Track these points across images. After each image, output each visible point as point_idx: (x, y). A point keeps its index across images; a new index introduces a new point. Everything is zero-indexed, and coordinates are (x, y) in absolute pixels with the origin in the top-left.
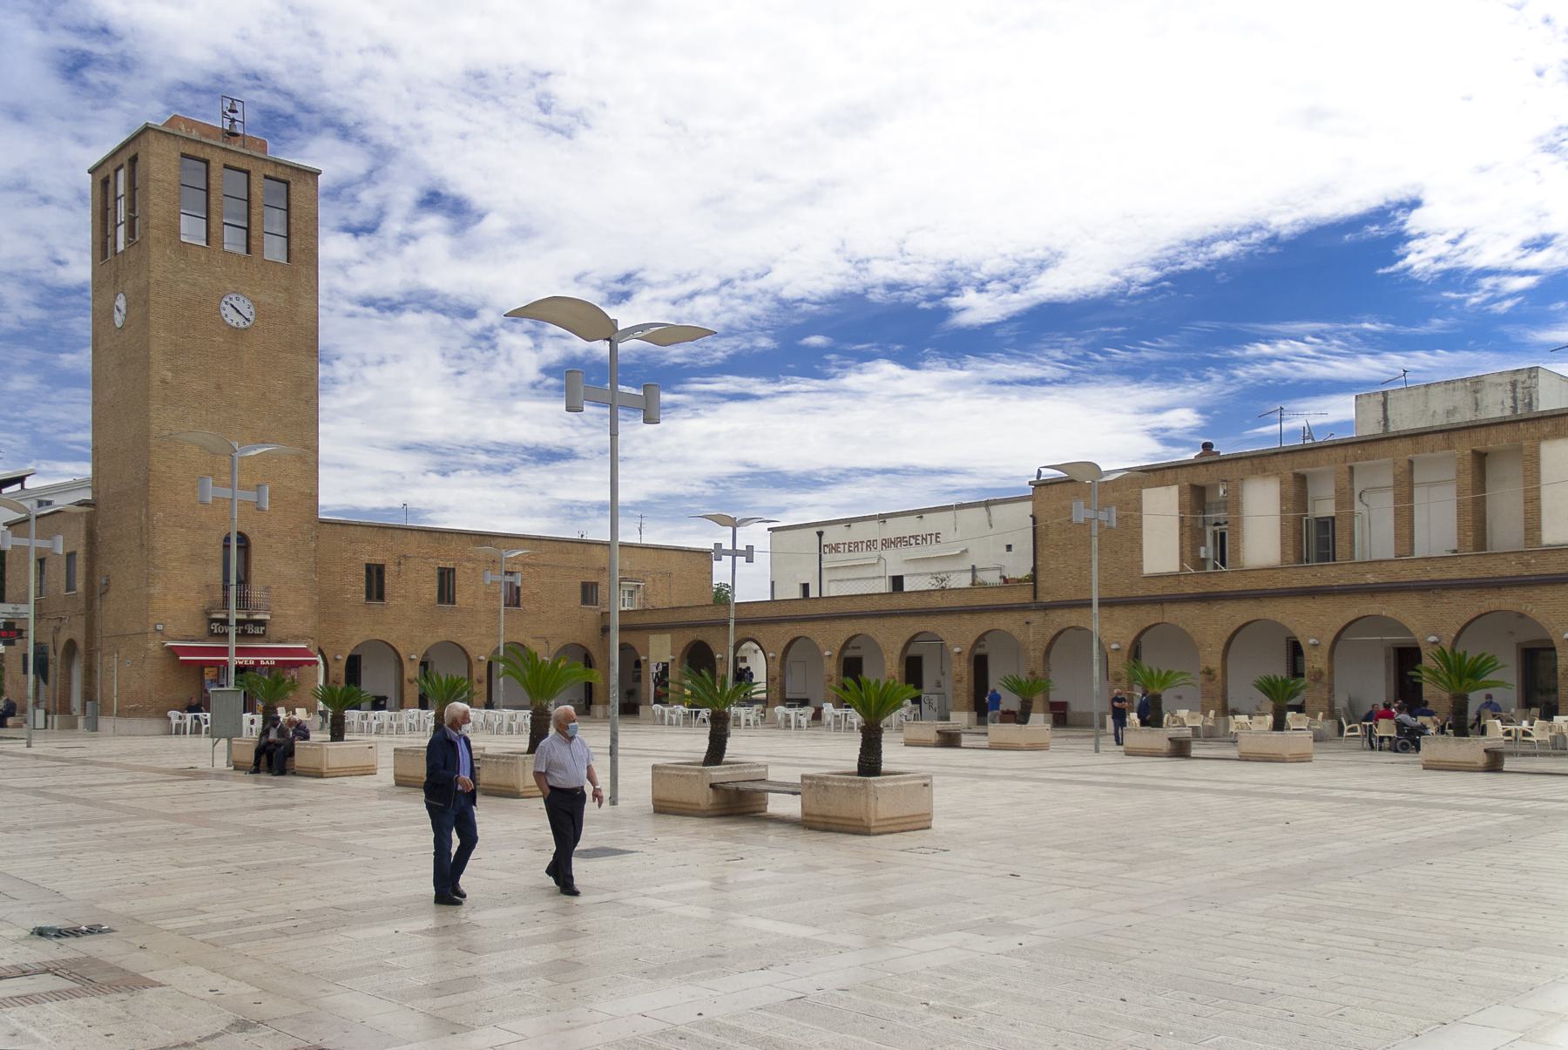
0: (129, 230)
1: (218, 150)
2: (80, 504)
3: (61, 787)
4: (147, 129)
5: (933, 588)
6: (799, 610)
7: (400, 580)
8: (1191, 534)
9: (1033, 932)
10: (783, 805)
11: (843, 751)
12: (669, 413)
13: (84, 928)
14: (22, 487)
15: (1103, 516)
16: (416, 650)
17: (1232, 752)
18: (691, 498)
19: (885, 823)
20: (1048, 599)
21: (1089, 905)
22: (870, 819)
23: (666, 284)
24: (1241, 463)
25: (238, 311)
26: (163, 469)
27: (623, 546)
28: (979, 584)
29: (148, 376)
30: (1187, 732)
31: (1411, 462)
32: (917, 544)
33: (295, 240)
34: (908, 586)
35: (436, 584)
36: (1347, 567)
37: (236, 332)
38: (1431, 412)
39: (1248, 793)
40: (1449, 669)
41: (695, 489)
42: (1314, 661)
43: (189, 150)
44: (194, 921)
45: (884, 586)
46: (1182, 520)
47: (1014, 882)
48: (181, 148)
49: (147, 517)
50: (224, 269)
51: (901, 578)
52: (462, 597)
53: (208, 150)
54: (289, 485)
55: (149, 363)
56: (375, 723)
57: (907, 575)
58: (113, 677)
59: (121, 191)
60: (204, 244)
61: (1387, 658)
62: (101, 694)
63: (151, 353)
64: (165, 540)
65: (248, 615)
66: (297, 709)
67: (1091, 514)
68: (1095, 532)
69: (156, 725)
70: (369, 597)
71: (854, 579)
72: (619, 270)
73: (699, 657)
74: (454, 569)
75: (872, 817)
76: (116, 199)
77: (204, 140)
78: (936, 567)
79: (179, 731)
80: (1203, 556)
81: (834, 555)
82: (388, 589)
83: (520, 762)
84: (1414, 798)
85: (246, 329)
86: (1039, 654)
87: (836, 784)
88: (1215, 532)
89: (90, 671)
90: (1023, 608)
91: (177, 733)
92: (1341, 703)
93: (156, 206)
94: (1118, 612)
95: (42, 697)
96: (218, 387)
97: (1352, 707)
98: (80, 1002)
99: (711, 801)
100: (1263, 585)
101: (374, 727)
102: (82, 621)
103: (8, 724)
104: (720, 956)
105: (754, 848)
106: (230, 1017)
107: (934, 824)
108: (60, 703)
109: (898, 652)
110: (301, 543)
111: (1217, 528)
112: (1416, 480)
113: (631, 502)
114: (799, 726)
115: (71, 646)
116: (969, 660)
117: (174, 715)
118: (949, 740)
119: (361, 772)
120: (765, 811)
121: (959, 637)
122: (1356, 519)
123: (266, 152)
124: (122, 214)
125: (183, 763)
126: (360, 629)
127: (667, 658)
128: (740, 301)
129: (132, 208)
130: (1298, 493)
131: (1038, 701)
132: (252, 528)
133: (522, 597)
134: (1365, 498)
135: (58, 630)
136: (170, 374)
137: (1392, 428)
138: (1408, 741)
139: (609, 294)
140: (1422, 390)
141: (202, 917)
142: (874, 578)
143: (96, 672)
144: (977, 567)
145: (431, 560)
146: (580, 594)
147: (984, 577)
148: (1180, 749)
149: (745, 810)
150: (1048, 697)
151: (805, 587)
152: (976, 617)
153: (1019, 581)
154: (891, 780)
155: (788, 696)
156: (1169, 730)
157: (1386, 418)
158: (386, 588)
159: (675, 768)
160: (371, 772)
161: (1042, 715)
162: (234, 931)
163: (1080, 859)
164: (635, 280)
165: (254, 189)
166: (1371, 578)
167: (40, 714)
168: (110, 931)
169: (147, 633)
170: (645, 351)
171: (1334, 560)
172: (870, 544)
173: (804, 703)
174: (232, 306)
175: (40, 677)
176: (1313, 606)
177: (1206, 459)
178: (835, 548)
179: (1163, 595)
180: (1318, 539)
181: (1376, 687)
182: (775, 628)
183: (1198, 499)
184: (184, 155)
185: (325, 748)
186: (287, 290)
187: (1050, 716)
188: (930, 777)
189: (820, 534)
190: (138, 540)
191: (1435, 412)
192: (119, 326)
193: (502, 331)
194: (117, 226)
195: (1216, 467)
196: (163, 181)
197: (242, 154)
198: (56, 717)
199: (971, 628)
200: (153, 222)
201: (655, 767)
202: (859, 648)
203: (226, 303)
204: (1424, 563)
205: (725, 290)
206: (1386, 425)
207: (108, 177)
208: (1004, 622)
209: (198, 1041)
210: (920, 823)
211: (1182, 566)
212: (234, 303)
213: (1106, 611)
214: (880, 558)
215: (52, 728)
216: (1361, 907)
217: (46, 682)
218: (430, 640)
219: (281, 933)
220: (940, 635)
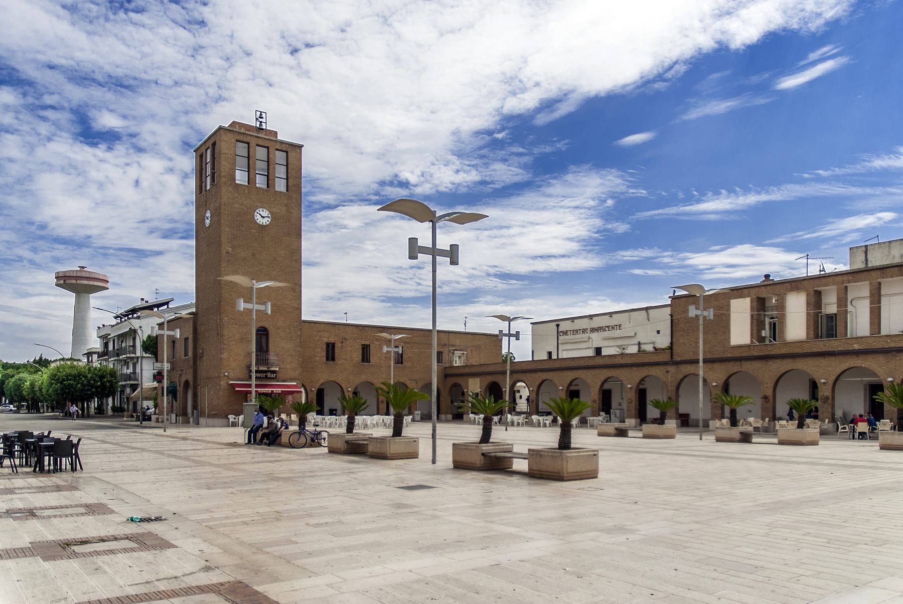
2: (190, 314)
3: (171, 450)
5: (618, 353)
6: (547, 366)
8: (757, 324)
9: (637, 533)
10: (521, 465)
11: (547, 437)
13: (153, 518)
14: (168, 307)
15: (705, 313)
17: (776, 440)
19: (573, 474)
20: (678, 359)
21: (672, 519)
22: (563, 472)
24: (785, 285)
26: (227, 296)
27: (438, 331)
28: (643, 351)
29: (220, 250)
30: (750, 429)
31: (880, 284)
32: (609, 330)
33: (290, 180)
34: (605, 352)
35: (361, 352)
36: (843, 341)
37: (262, 227)
38: (892, 257)
39: (777, 461)
40: (896, 395)
42: (824, 391)
43: (240, 138)
44: (206, 516)
45: (591, 353)
46: (752, 316)
47: (635, 507)
51: (600, 348)
52: (373, 360)
53: (249, 137)
56: (328, 422)
57: (604, 347)
60: (247, 184)
61: (865, 390)
65: (268, 368)
67: (699, 312)
68: (701, 322)
70: (327, 359)
71: (575, 349)
73: (495, 390)
75: (565, 471)
76: (206, 164)
77: (247, 132)
78: (619, 342)
80: (763, 335)
81: (565, 337)
82: (336, 355)
83: (388, 441)
84: (870, 464)
85: (267, 226)
86: (674, 388)
87: (546, 454)
88: (770, 323)
89: (195, 396)
90: (665, 363)
91: (233, 426)
92: (839, 414)
94: (717, 366)
95: (174, 408)
96: (253, 255)
97: (845, 415)
98: (135, 554)
99: (482, 462)
100: (800, 351)
101: (328, 424)
102: (191, 371)
104: (462, 542)
105: (500, 487)
106: (204, 564)
107: (599, 475)
109: (598, 387)
111: (771, 320)
112: (882, 293)
114: (545, 426)
115: (187, 383)
116: (636, 391)
117: (231, 418)
118: (622, 433)
120: (512, 468)
121: (630, 380)
122: (849, 315)
123: (277, 137)
124: (209, 172)
125: (232, 440)
126: (323, 375)
127: (478, 390)
129: (213, 168)
130: (815, 301)
131: (670, 412)
134: (854, 303)
135: (181, 375)
136: (230, 249)
137: (870, 265)
138: (870, 435)
140: (887, 244)
141: (211, 514)
142: (586, 349)
144: (641, 342)
145: (358, 341)
147: (644, 347)
148: (745, 438)
149: (502, 467)
150: (677, 409)
151: (550, 354)
152: (640, 368)
153: (663, 349)
154: (576, 452)
155: (540, 410)
156: (742, 428)
157: (866, 260)
160: (592, 476)
161: (675, 421)
162: (223, 522)
163: (674, 495)
166: (856, 347)
168: (165, 519)
171: (836, 337)
172: (584, 331)
173: (549, 414)
176: (824, 361)
177: (766, 283)
178: (565, 333)
179: (742, 356)
180: (827, 326)
181: (858, 405)
182: (533, 375)
183: (760, 305)
186: (286, 205)
187: (679, 421)
188: (597, 451)
189: (558, 326)
190: (216, 331)
191: (894, 256)
194: (207, 177)
195: (771, 287)
196: (227, 154)
197: (265, 139)
198: (181, 418)
199: (637, 375)
200: (223, 174)
201: (454, 445)
202: (578, 385)
203: (257, 213)
204: (886, 338)
206: (867, 263)
208: (655, 371)
209: (183, 576)
210: (592, 475)
211: (752, 341)
212: (261, 213)
213: (710, 365)
214: (589, 338)
216: (825, 522)
217: (176, 401)
218: (357, 381)
219: (246, 523)
220: (620, 378)
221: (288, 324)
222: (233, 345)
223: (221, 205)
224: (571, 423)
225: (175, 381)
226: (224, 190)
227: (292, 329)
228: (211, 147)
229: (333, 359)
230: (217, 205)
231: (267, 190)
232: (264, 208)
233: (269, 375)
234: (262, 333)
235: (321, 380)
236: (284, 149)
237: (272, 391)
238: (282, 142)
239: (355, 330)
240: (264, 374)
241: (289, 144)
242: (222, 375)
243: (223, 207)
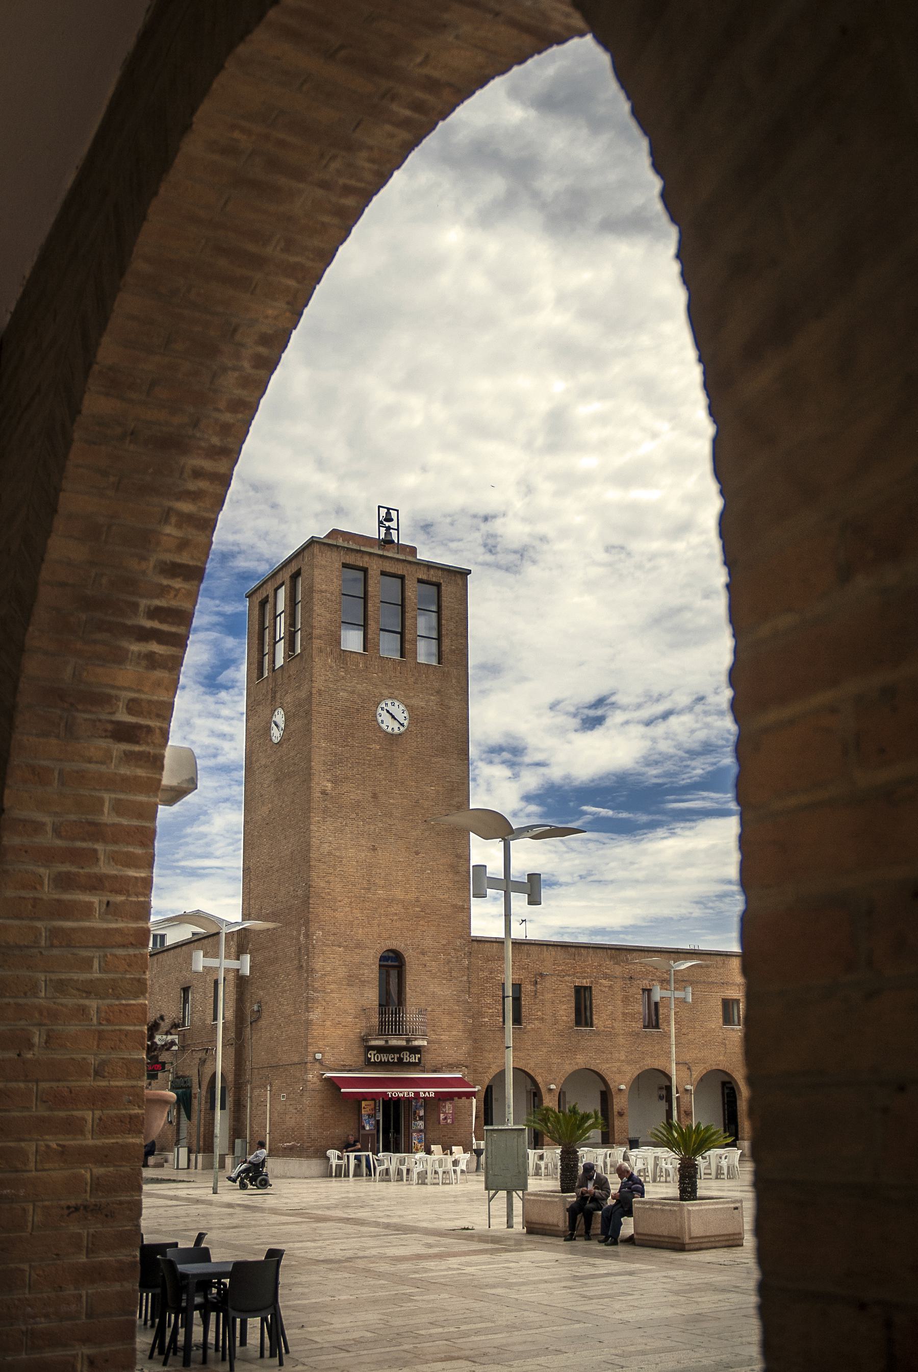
0: (290, 645)
1: (376, 558)
4: (313, 542)
7: (537, 1001)
12: (646, 834)
16: (555, 1079)
18: (679, 920)
23: (639, 706)
25: (393, 717)
26: (322, 884)
29: (309, 788)
33: (446, 642)
37: (392, 738)
41: (683, 911)
43: (350, 559)
48: (342, 558)
49: (307, 936)
50: (380, 674)
53: (366, 558)
54: (442, 897)
55: (310, 774)
58: (265, 1113)
59: (281, 607)
62: (251, 1131)
63: (313, 763)
64: (324, 961)
65: (408, 1041)
66: (453, 1147)
69: (314, 1165)
72: (590, 696)
74: (590, 987)
79: (341, 1173)
91: (338, 1175)
93: (322, 615)
96: (375, 796)
103: (149, 1164)
108: (205, 1141)
113: (622, 927)
117: (332, 1154)
119: (727, 1243)
124: (281, 628)
128: (716, 717)
132: (406, 945)
136: (329, 785)
139: (583, 720)
143: (245, 1106)
145: (567, 978)
146: (721, 1013)
158: (523, 1010)
159: (550, 1196)
160: (735, 1243)
164: (607, 705)
165: (409, 594)
167: (183, 1152)
169: (306, 1063)
170: (624, 773)
174: (388, 711)
175: (182, 1110)
184: (345, 566)
185: (685, 1208)
186: (438, 692)
192: (276, 741)
193: (481, 764)
194: (276, 643)
197: (398, 560)
200: (317, 632)
205: (699, 708)
207: (267, 596)
212: (390, 708)
215: (196, 1168)
221: (444, 942)
223: (311, 693)
225: (187, 1073)
226: (318, 662)
227: (453, 953)
228: (288, 582)
230: (303, 695)
231: (401, 662)
232: (395, 698)
233: (407, 1057)
234: (390, 963)
235: (493, 1066)
236: (434, 579)
237: (417, 1094)
238: (429, 566)
239: (560, 954)
241: (442, 569)
242: (310, 1058)
243: (316, 699)
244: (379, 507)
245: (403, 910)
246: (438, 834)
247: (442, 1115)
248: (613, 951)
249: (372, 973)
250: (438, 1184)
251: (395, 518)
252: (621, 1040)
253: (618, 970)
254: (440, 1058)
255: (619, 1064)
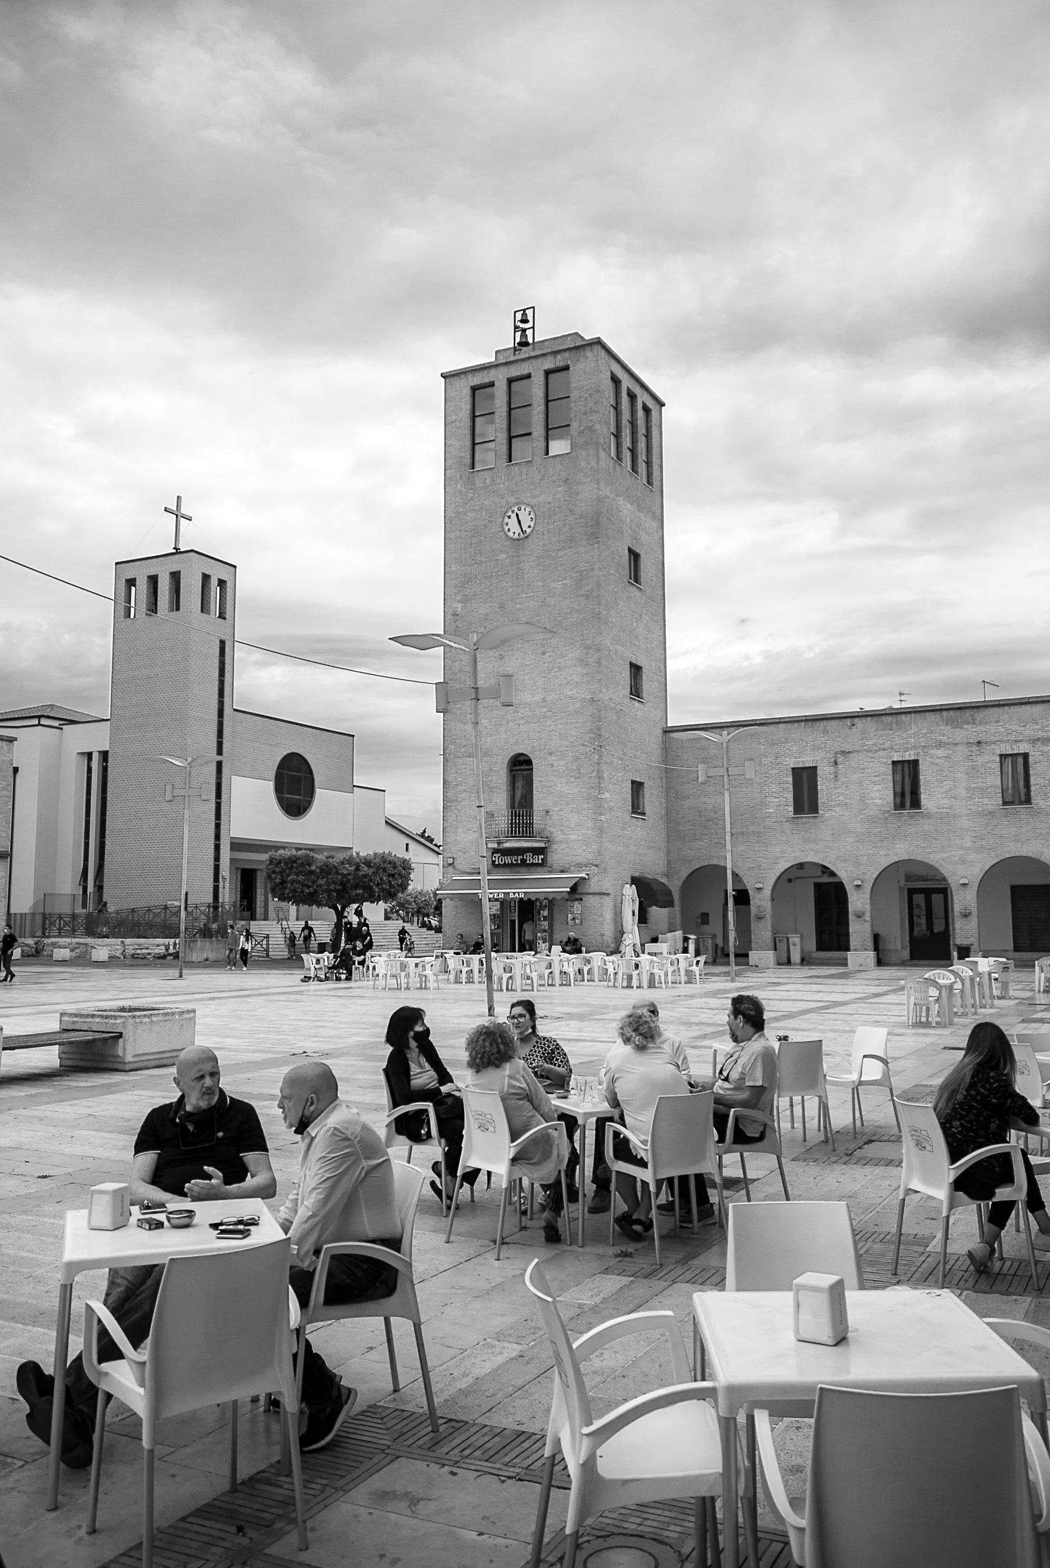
7: (839, 784)
50: (506, 483)
54: (570, 693)
65: (499, 843)
82: (822, 797)
96: (502, 606)
110: (582, 757)
133: (1033, 788)
136: (460, 606)
145: (880, 753)
174: (517, 515)
222: (463, 799)
224: (390, 1049)
229: (814, 808)
240: (520, 857)
244: (533, 308)
245: (529, 713)
246: (566, 629)
247: (570, 915)
248: (951, 713)
249: (501, 777)
250: (544, 985)
251: (530, 318)
252: (964, 823)
253: (960, 735)
254: (568, 858)
255: (961, 852)
